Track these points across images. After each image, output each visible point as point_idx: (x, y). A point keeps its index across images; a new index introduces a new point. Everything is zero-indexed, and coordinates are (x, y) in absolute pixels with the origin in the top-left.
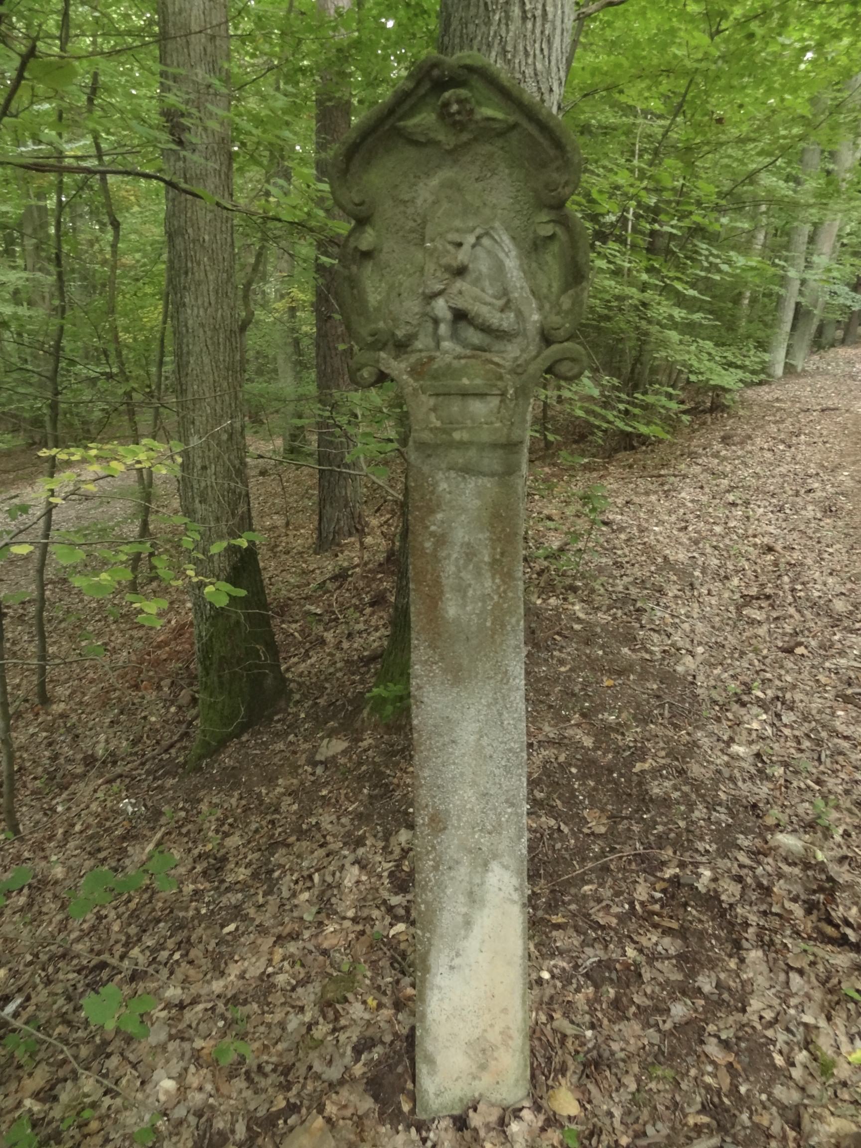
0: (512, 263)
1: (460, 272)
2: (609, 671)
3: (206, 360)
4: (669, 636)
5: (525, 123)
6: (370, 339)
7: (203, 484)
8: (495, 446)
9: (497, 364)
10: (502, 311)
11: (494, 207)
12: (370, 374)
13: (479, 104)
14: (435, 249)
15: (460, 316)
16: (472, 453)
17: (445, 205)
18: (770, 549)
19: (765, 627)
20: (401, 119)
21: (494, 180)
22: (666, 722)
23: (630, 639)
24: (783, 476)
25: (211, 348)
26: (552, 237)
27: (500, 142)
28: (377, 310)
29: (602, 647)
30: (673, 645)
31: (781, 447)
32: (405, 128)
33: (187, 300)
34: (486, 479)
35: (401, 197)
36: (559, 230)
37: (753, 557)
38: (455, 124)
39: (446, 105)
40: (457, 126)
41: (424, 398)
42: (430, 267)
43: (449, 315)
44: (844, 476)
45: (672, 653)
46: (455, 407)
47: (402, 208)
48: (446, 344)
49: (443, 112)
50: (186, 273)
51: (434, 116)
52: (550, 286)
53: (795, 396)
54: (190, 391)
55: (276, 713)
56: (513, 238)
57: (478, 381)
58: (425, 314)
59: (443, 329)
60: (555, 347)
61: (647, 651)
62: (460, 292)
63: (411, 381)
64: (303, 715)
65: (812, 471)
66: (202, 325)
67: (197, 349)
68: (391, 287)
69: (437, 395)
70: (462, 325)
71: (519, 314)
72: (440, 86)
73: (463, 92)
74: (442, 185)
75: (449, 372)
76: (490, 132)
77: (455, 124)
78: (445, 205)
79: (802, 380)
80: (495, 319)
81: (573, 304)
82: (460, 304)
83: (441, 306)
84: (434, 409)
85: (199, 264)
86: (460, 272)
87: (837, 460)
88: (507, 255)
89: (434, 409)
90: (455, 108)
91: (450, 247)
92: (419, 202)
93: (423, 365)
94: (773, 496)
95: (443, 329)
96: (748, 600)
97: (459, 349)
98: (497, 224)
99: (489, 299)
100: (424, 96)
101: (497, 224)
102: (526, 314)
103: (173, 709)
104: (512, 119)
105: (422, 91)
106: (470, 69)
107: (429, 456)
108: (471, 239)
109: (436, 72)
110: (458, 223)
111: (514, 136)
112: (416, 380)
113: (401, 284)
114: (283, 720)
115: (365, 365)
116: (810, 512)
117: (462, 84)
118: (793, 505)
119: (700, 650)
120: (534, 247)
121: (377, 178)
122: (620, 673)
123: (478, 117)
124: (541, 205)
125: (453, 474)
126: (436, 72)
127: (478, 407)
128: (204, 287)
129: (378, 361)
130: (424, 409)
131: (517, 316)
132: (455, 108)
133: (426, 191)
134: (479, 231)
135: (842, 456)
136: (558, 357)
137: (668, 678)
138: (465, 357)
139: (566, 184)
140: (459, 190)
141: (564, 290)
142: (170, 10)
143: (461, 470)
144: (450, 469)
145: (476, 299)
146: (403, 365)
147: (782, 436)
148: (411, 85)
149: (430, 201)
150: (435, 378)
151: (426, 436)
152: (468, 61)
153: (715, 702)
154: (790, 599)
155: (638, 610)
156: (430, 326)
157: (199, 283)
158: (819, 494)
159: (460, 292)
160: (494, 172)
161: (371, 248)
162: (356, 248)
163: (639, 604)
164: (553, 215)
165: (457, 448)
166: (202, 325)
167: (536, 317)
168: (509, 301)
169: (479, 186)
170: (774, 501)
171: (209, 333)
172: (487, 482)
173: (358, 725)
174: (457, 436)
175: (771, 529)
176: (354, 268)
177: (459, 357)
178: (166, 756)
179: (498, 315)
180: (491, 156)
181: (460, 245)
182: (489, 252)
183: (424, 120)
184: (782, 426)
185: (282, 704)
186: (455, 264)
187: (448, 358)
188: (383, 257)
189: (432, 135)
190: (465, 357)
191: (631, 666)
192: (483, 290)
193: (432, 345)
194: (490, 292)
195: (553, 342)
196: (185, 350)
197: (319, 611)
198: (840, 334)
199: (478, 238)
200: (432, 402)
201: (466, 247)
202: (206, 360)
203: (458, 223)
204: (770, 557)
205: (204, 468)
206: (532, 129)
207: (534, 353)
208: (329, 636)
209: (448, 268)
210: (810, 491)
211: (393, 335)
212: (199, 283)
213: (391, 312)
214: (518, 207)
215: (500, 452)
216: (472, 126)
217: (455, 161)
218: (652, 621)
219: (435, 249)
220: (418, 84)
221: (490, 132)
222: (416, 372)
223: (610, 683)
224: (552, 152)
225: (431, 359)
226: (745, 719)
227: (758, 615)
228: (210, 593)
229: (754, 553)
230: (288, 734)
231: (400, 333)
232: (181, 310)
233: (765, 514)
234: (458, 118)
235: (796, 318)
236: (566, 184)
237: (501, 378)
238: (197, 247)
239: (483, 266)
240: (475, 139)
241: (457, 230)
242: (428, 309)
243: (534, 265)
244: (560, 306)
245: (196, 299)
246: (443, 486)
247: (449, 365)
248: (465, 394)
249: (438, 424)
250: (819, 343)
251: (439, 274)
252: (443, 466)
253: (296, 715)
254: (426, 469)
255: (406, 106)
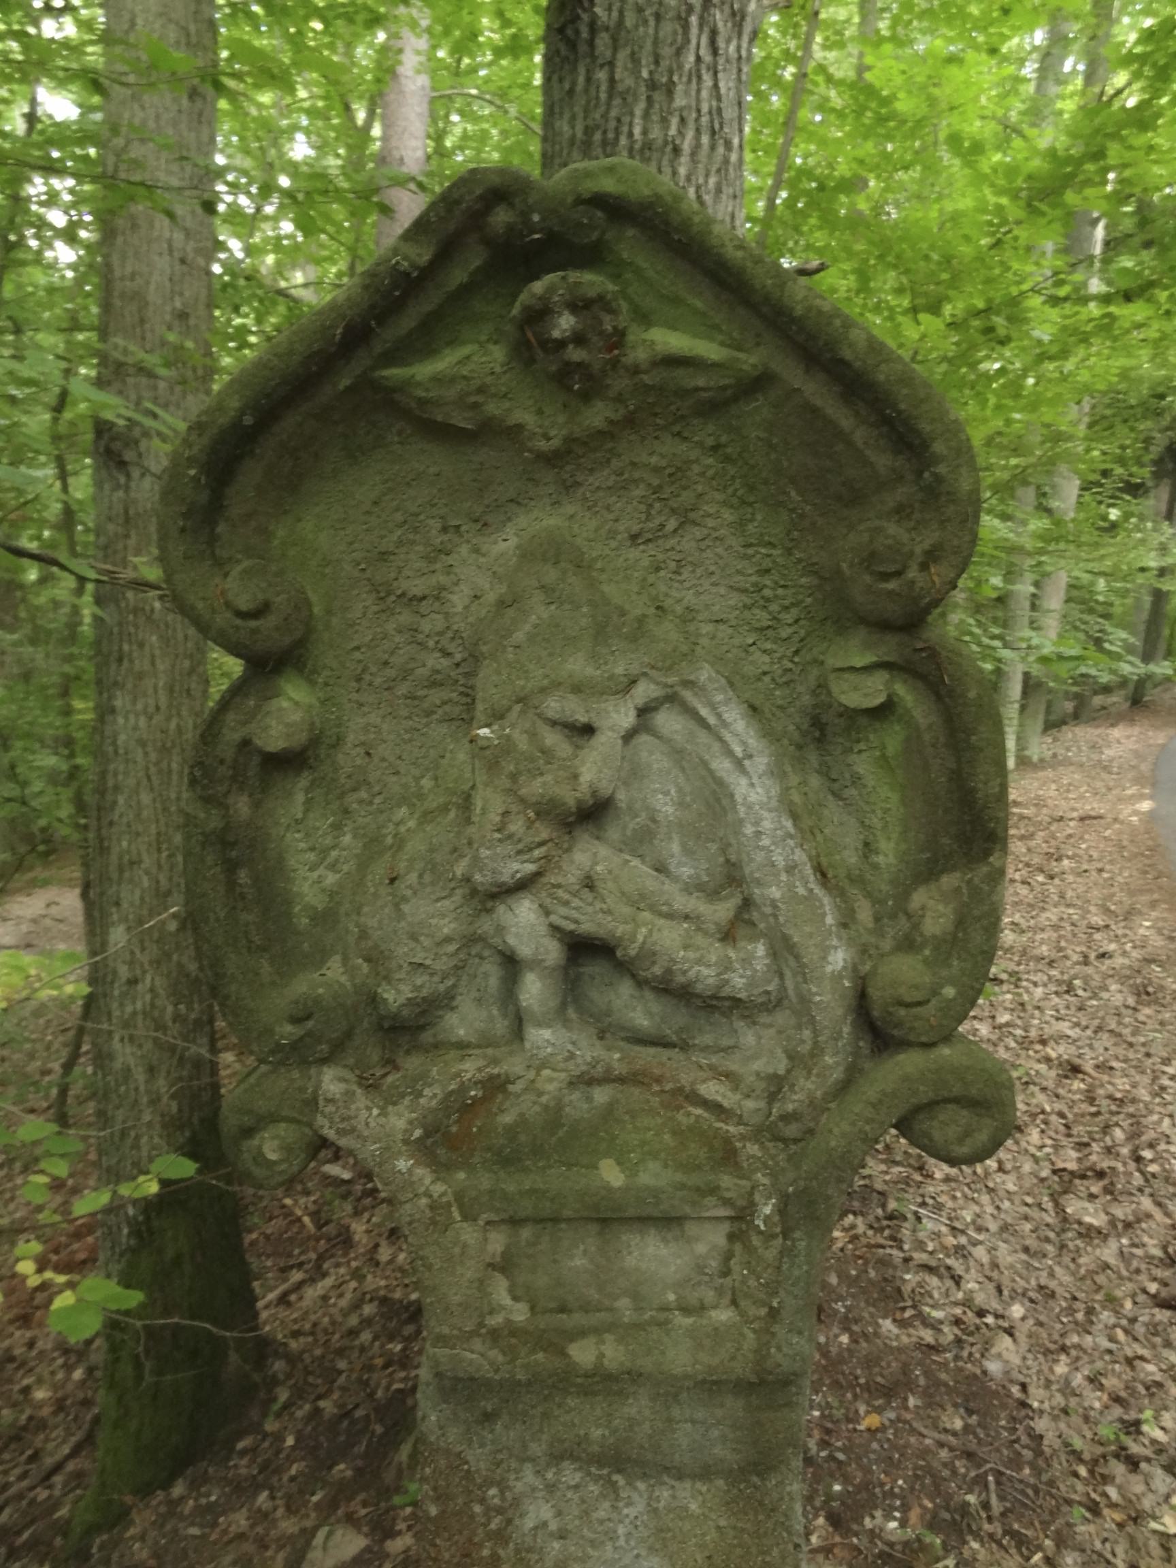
0: (755, 791)
1: (593, 814)
2: (867, 1388)
3: (146, 798)
4: (957, 1280)
5: (792, 374)
6: (287, 1031)
7: (129, 1009)
8: (711, 1386)
9: (716, 1108)
10: (727, 936)
11: (689, 615)
12: (287, 1149)
13: (645, 319)
14: (507, 747)
15: (584, 950)
16: (638, 1406)
17: (539, 611)
18: (1076, 1070)
19: (1113, 1244)
20: (391, 357)
21: (688, 542)
22: (996, 1528)
23: (889, 1296)
24: (1056, 927)
25: (156, 781)
26: (884, 711)
27: (707, 432)
28: (326, 918)
29: (846, 1324)
30: (967, 1303)
31: (1041, 878)
32: (404, 386)
33: (118, 703)
34: (685, 1489)
35: (403, 585)
36: (905, 692)
37: (1050, 1084)
38: (564, 375)
39: (539, 315)
40: (574, 382)
41: (469, 1234)
42: (490, 802)
43: (553, 952)
44: (1144, 927)
45: (975, 1328)
46: (578, 1258)
47: (405, 617)
48: (542, 1037)
49: (530, 342)
50: (120, 660)
51: (498, 354)
52: (868, 847)
53: (1038, 797)
54: (115, 851)
55: (240, 1435)
56: (754, 709)
57: (653, 1175)
58: (472, 940)
59: (534, 990)
60: (909, 1062)
61: (927, 1322)
62: (589, 883)
63: (424, 1175)
64: (290, 1441)
65: (1098, 920)
66: (142, 743)
67: (131, 782)
68: (373, 845)
69: (515, 1222)
70: (594, 969)
71: (783, 949)
72: (519, 257)
73: (591, 281)
74: (526, 555)
75: (557, 1139)
76: (675, 401)
77: (567, 372)
78: (539, 611)
79: (1041, 774)
80: (704, 965)
81: (960, 922)
82: (589, 920)
83: (524, 924)
84: (505, 1265)
85: (141, 645)
86: (593, 814)
87: (1127, 901)
88: (739, 764)
89: (505, 1265)
90: (565, 323)
91: (551, 738)
92: (458, 600)
93: (467, 1109)
94: (1051, 963)
95: (534, 990)
96: (1066, 1181)
97: (589, 1051)
98: (705, 674)
99: (682, 902)
100: (465, 291)
101: (705, 674)
102: (810, 955)
103: (78, 1374)
104: (750, 361)
105: (458, 276)
106: (615, 209)
107: (488, 1418)
108: (623, 716)
109: (501, 218)
110: (577, 665)
111: (758, 410)
112: (441, 1168)
113: (400, 843)
114: (253, 1451)
115: (273, 1118)
116: (1117, 995)
117: (592, 256)
118: (1086, 979)
119: (1017, 1310)
120: (820, 735)
121: (331, 533)
122: (890, 1392)
123: (640, 355)
124: (838, 611)
125: (571, 1475)
126: (501, 218)
127: (655, 1258)
128: (148, 683)
129: (312, 1104)
130: (469, 1271)
131: (774, 954)
132: (565, 323)
133: (481, 568)
134: (644, 691)
135: (1132, 893)
136: (926, 1093)
137: (977, 1395)
138: (608, 1079)
139: (932, 556)
140: (581, 565)
141: (927, 870)
142: (118, 273)
143: (599, 1460)
144: (557, 1458)
145: (641, 901)
146: (399, 1120)
147: (1036, 860)
148: (423, 255)
149: (491, 597)
150: (508, 1160)
151: (478, 1358)
152: (608, 185)
153: (1077, 1456)
154: (1138, 1180)
155: (890, 1217)
156: (492, 973)
157: (140, 676)
158: (1119, 961)
159: (589, 883)
160: (686, 517)
161: (302, 738)
162: (246, 743)
163: (892, 1205)
164: (889, 648)
165: (586, 1392)
166: (142, 743)
167: (839, 958)
168: (747, 903)
169: (640, 556)
170: (1054, 972)
171: (153, 756)
172: (691, 1498)
173: (389, 1477)
174: (583, 1354)
175: (1064, 1027)
176: (242, 806)
177: (585, 1081)
178: (42, 1494)
179: (715, 952)
180: (678, 473)
181: (588, 730)
182: (678, 754)
183: (466, 363)
184: (1032, 843)
185: (254, 1413)
186: (570, 797)
187: (551, 1083)
188: (348, 758)
189: (493, 408)
190: (608, 1079)
191: (905, 1370)
192: (661, 869)
193: (501, 1026)
194: (686, 872)
195: (904, 1044)
196: (110, 783)
197: (346, 1176)
198: (1069, 706)
199: (644, 712)
200: (497, 1242)
201: (607, 741)
202: (146, 798)
203: (577, 665)
204: (1077, 1085)
205: (133, 982)
206: (814, 390)
207: (837, 1075)
208: (358, 1228)
209: (546, 810)
210: (1103, 955)
211: (374, 1000)
212: (140, 676)
213: (364, 934)
214: (762, 618)
215: (734, 1405)
216: (619, 383)
217: (569, 487)
218: (920, 1245)
219: (507, 747)
220: (447, 251)
221: (675, 401)
222: (442, 1141)
223: (873, 1420)
224: (883, 461)
225: (496, 1086)
226: (1147, 1504)
227: (1094, 1217)
228: (67, 1310)
229: (1050, 1075)
230: (257, 1488)
231: (395, 996)
232: (109, 718)
233: (1046, 998)
234: (575, 354)
235: (1025, 693)
236: (932, 556)
237: (727, 1156)
238: (142, 620)
239: (663, 798)
240: (630, 422)
241: (577, 689)
242: (485, 926)
243: (815, 781)
244: (915, 921)
245: (134, 701)
246: (538, 1512)
247: (554, 1116)
248: (610, 1217)
249: (520, 1313)
250: (1052, 725)
251: (516, 826)
252: (536, 1449)
253: (279, 1437)
254: (477, 1458)
255: (407, 322)
